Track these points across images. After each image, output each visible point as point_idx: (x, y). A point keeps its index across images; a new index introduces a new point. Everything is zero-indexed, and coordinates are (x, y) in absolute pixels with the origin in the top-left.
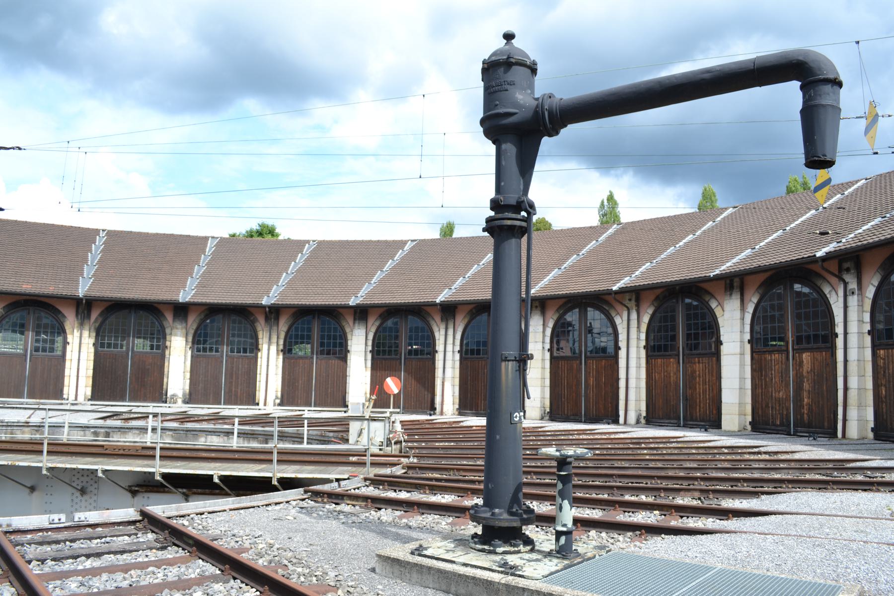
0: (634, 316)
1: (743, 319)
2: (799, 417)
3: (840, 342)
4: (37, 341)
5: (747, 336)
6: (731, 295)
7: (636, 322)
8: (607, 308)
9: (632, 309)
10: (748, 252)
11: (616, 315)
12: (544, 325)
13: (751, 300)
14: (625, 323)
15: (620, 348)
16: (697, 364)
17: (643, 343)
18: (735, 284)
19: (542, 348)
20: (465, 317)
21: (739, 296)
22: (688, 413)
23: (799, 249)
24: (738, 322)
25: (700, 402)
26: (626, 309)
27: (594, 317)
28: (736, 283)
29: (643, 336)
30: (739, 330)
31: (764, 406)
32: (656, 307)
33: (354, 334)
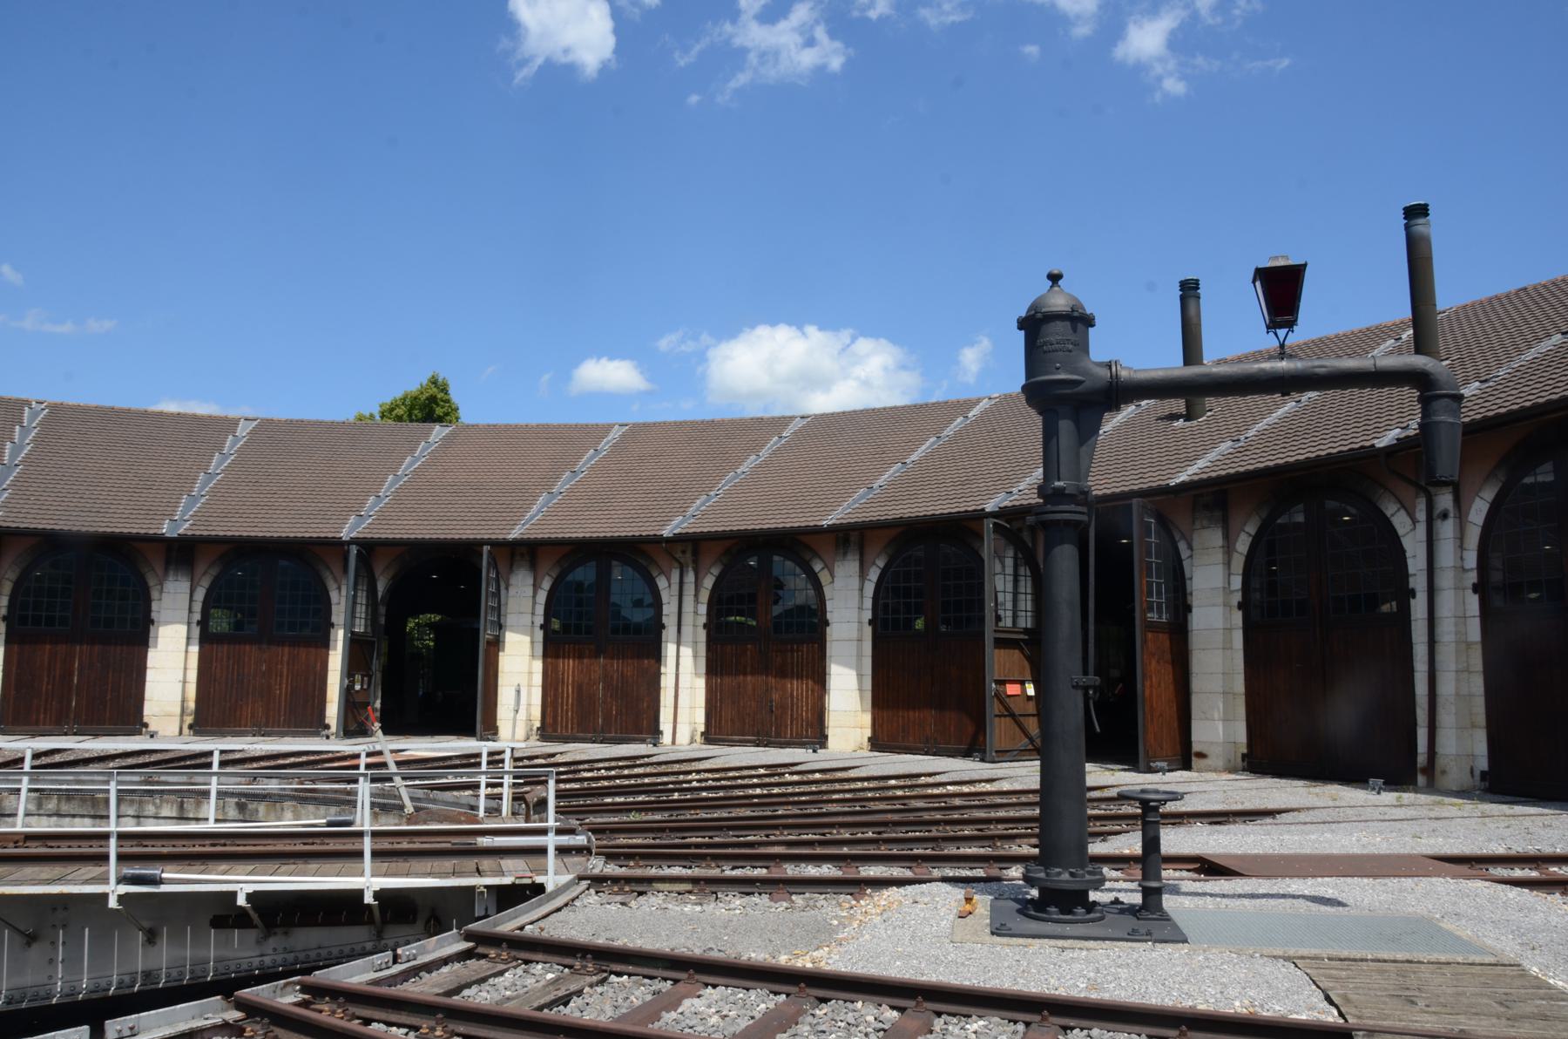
0: (690, 577)
1: (861, 590)
3: (1419, 607)
5: (868, 615)
6: (845, 554)
7: (693, 586)
8: (645, 563)
9: (688, 567)
10: (1226, 446)
11: (659, 574)
12: (534, 585)
13: (874, 563)
14: (675, 587)
16: (789, 654)
17: (703, 620)
18: (852, 539)
19: (530, 624)
21: (857, 557)
23: (1285, 450)
24: (856, 593)
26: (676, 565)
27: (782, 565)
28: (854, 537)
29: (703, 609)
30: (857, 606)
33: (165, 590)
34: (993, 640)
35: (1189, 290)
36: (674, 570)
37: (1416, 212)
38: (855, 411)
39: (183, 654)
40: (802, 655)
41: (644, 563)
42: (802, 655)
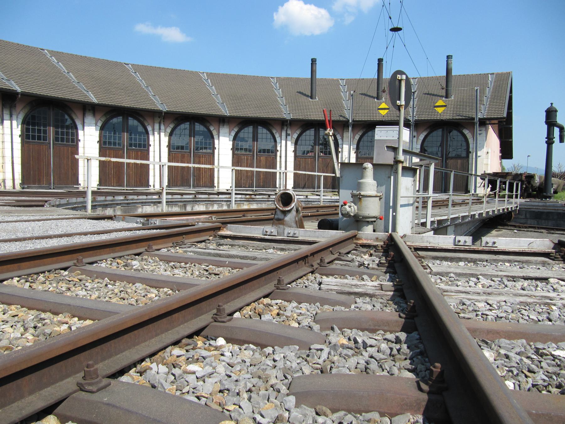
2: (258, 184)
4: (131, 139)
6: (223, 125)
13: (233, 129)
15: (150, 145)
20: (24, 107)
22: (196, 183)
25: (203, 178)
31: (239, 179)
32: (176, 124)
34: (532, 172)
35: (313, 61)
36: (155, 124)
37: (449, 57)
38: (223, 74)
39: (220, 153)
40: (206, 159)
41: (142, 119)
42: (206, 159)
